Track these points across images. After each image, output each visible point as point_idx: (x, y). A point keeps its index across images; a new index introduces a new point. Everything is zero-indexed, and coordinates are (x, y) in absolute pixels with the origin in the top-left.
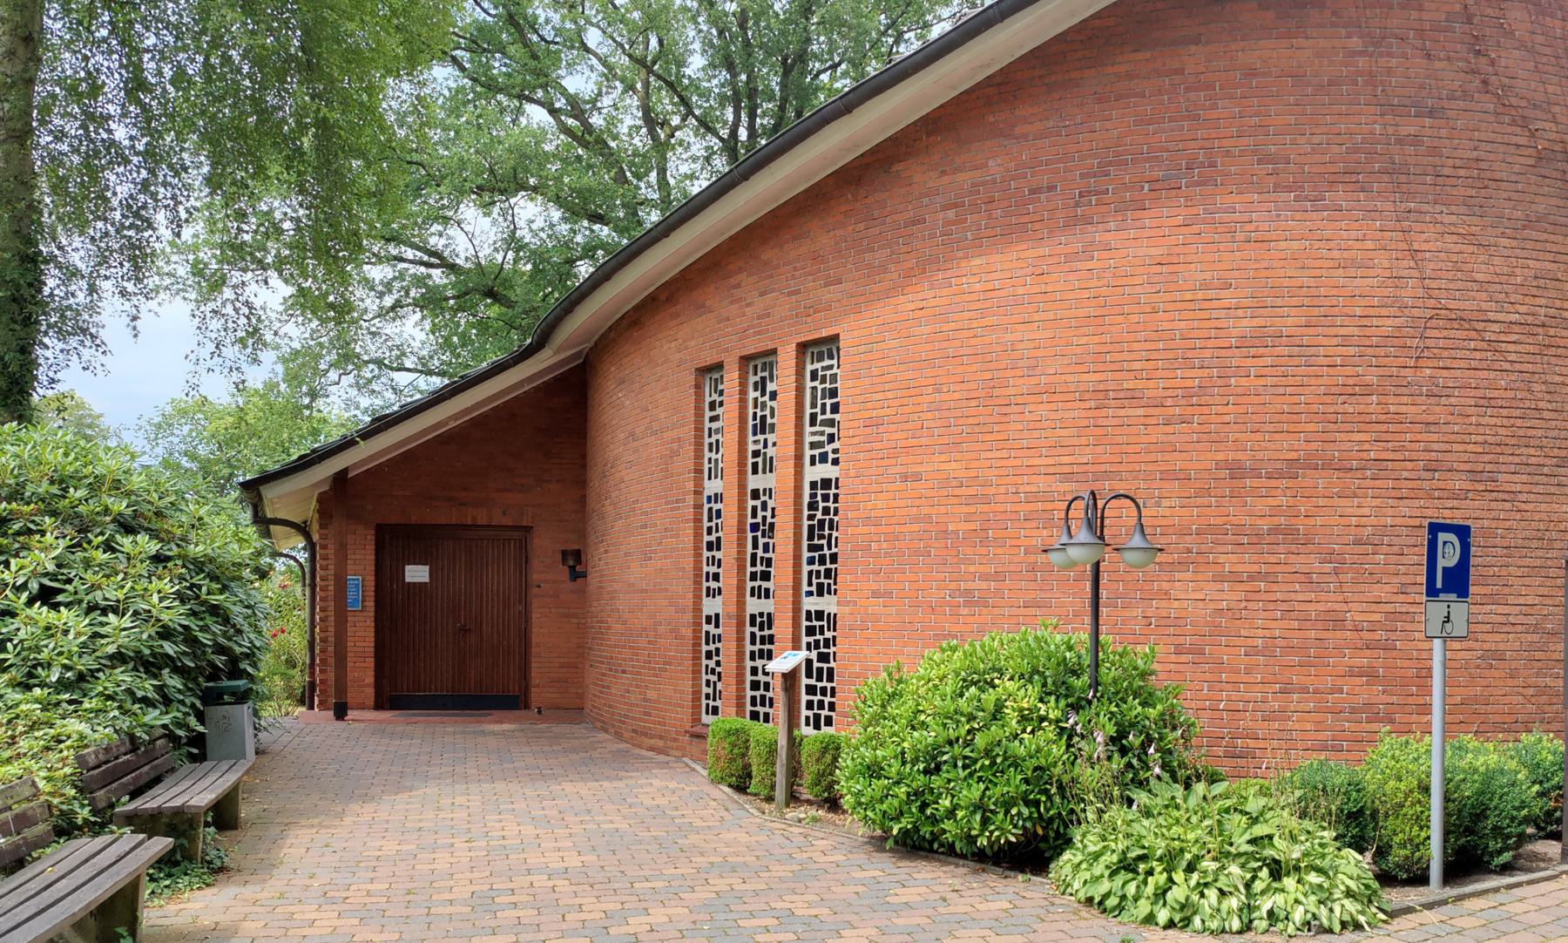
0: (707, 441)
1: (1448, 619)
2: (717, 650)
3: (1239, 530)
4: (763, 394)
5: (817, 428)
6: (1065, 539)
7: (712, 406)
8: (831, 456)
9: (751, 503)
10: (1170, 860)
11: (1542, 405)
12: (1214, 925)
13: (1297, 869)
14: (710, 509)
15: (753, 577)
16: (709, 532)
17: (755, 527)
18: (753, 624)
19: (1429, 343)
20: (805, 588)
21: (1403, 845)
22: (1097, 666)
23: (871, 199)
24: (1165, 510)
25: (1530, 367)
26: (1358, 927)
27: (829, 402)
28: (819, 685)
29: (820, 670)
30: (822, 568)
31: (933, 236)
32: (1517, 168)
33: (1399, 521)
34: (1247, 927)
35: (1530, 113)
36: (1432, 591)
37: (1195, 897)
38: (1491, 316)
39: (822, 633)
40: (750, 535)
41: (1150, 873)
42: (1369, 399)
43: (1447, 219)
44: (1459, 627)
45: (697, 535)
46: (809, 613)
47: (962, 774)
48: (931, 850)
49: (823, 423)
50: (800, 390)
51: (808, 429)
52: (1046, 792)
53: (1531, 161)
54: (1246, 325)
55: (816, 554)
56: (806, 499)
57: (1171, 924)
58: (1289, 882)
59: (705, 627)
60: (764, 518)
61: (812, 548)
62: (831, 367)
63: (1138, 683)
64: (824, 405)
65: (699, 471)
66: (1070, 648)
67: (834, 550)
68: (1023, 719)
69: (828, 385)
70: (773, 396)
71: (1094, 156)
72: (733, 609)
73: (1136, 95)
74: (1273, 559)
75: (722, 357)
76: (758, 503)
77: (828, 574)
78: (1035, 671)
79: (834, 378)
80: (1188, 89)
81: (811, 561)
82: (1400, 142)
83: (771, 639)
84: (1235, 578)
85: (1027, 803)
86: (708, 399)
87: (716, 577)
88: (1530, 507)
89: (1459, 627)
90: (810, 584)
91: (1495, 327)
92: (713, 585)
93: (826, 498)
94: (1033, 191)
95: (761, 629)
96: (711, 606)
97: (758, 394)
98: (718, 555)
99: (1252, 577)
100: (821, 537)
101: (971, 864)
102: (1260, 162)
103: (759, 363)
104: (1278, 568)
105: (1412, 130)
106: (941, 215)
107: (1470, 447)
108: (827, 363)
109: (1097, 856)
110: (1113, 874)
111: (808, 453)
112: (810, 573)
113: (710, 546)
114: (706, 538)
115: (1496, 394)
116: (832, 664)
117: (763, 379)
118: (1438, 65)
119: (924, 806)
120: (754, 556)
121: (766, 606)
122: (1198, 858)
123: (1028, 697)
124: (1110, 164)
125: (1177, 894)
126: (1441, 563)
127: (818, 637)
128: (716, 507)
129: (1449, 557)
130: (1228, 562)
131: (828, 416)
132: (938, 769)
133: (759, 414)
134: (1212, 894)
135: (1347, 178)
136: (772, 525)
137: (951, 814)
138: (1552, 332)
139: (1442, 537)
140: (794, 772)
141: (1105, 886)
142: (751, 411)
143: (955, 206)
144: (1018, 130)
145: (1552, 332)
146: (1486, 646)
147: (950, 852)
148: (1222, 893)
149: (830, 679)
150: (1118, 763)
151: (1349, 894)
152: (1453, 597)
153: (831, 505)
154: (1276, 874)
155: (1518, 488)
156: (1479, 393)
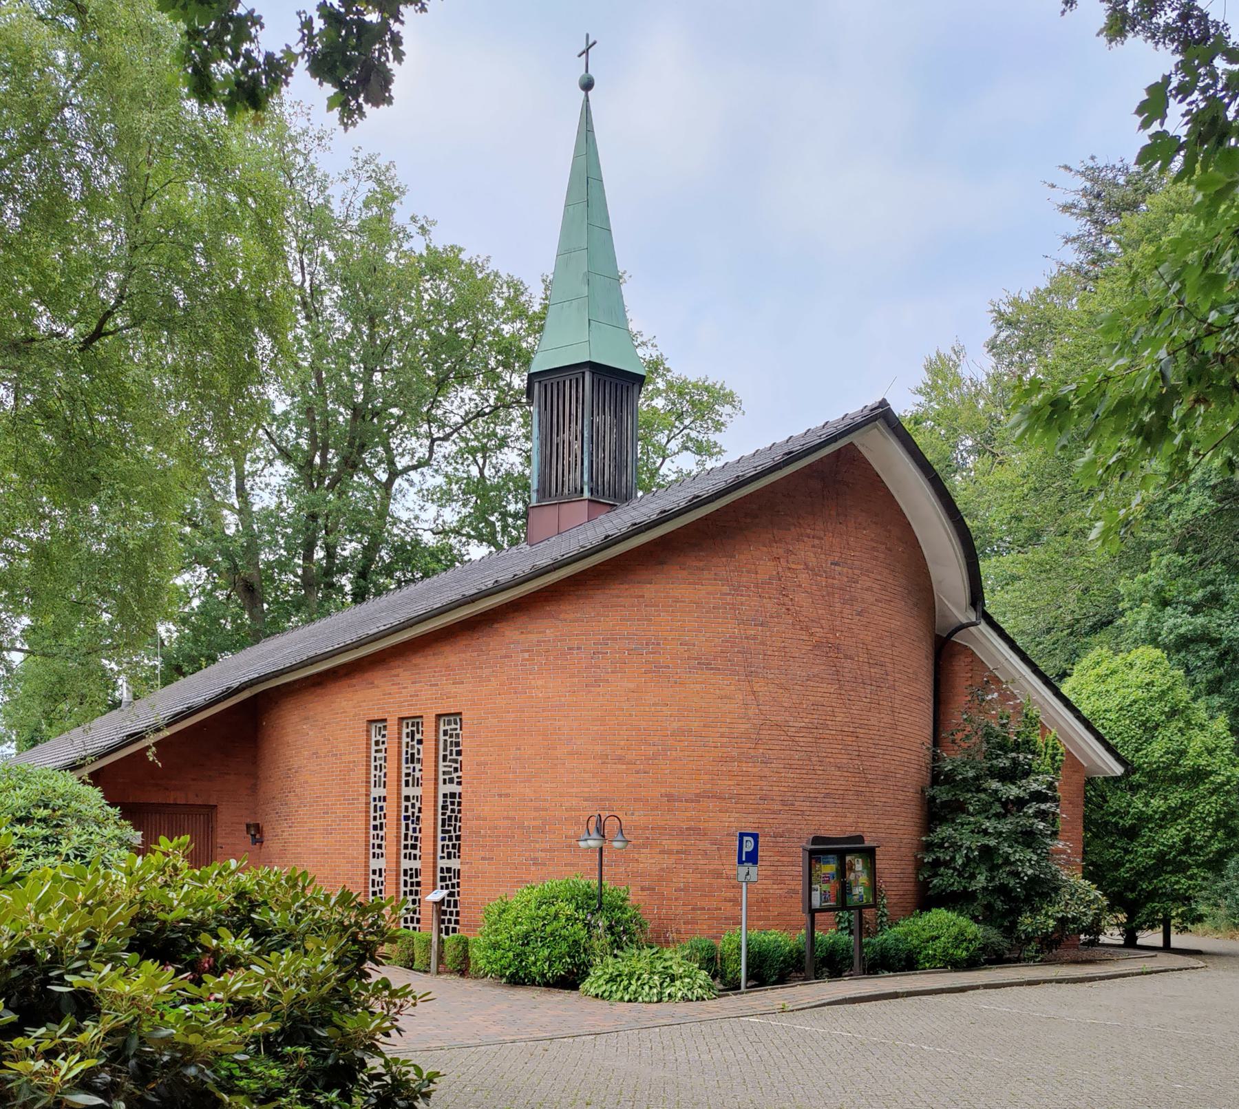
0: (373, 764)
1: (748, 874)
2: (458, 883)
4: (413, 740)
5: (447, 763)
6: (586, 836)
7: (377, 743)
9: (404, 804)
10: (630, 976)
11: (816, 767)
12: (647, 999)
13: (681, 977)
14: (375, 806)
15: (406, 847)
16: (375, 818)
17: (407, 818)
18: (405, 874)
19: (762, 737)
20: (440, 854)
21: (730, 973)
22: (601, 895)
23: (481, 640)
24: (635, 817)
25: (810, 749)
26: (704, 999)
27: (455, 749)
28: (449, 910)
29: (449, 901)
30: (450, 843)
31: (516, 665)
33: (748, 824)
34: (660, 1001)
35: (810, 624)
36: (741, 862)
37: (640, 989)
38: (791, 724)
39: (450, 880)
40: (403, 823)
41: (622, 980)
42: (733, 764)
44: (753, 877)
45: (367, 821)
46: (442, 869)
47: (540, 945)
48: (524, 984)
49: (451, 761)
50: (437, 740)
51: (441, 763)
53: (810, 648)
54: (675, 725)
55: (447, 835)
56: (440, 803)
57: (630, 1001)
58: (678, 983)
59: (372, 877)
60: (413, 813)
61: (443, 831)
62: (456, 729)
64: (451, 750)
66: (589, 887)
67: (458, 833)
68: (567, 919)
69: (454, 740)
71: (601, 634)
73: (621, 606)
76: (409, 804)
77: (454, 846)
80: (646, 606)
81: (443, 839)
82: (747, 638)
83: (418, 884)
84: (670, 852)
85: (570, 957)
86: (374, 739)
87: (380, 846)
88: (811, 818)
89: (753, 877)
90: (443, 852)
91: (793, 729)
92: (377, 851)
93: (452, 803)
94: (570, 649)
95: (411, 878)
96: (375, 864)
97: (409, 740)
98: (381, 833)
99: (678, 852)
101: (543, 988)
102: (681, 644)
103: (410, 722)
105: (753, 632)
106: (521, 655)
107: (782, 789)
108: (453, 726)
109: (600, 977)
110: (607, 983)
111: (441, 777)
112: (443, 846)
113: (375, 828)
114: (373, 823)
115: (794, 762)
116: (457, 898)
117: (413, 732)
119: (522, 961)
120: (406, 835)
121: (416, 864)
122: (641, 974)
123: (569, 909)
124: (608, 639)
125: (633, 988)
126: (745, 850)
127: (448, 882)
129: (749, 846)
130: (667, 843)
131: (454, 757)
132: (528, 944)
133: (410, 752)
134: (646, 988)
135: (722, 655)
136: (418, 818)
137: (534, 963)
138: (821, 731)
139: (745, 838)
140: (441, 958)
142: (404, 749)
143: (528, 651)
144: (561, 616)
145: (821, 731)
146: (790, 887)
147: (533, 983)
148: (651, 988)
149: (455, 906)
150: (609, 938)
151: (700, 987)
152: (750, 864)
153: (456, 808)
154: (673, 980)
155: (805, 808)
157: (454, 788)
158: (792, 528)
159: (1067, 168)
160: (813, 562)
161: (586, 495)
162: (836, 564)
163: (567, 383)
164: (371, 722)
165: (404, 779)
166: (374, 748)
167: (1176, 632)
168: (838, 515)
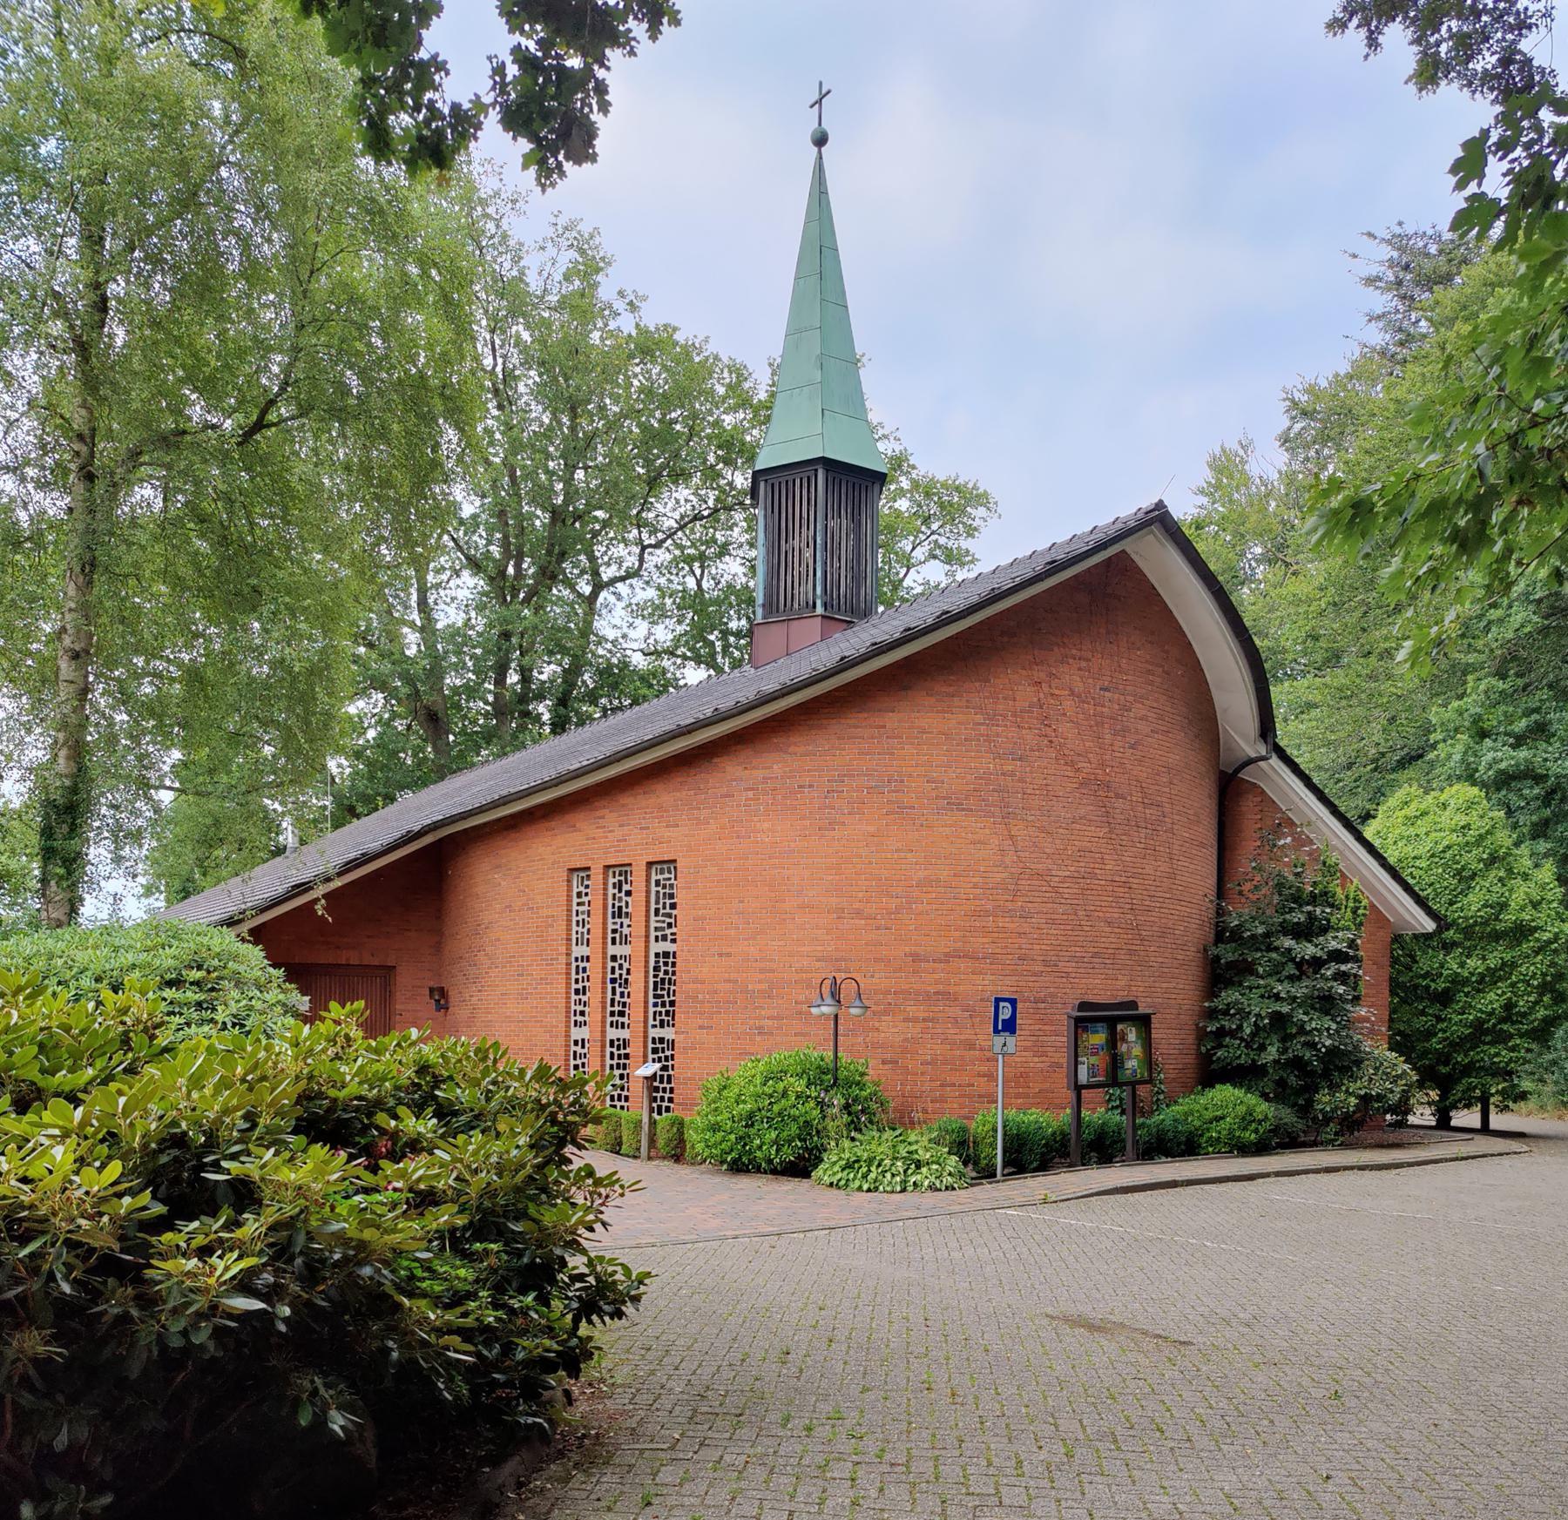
1: (1005, 1045)
3: (918, 993)
4: (620, 891)
5: (660, 918)
6: (819, 1002)
7: (579, 895)
8: (670, 937)
9: (610, 964)
10: (870, 1161)
14: (577, 967)
15: (612, 1014)
17: (613, 981)
20: (651, 1022)
24: (876, 980)
25: (1076, 902)
26: (954, 1189)
30: (663, 1010)
32: (1068, 790)
34: (904, 1190)
35: (1076, 758)
36: (996, 1031)
37: (880, 1177)
38: (1054, 873)
39: (663, 1052)
40: (609, 986)
41: (860, 1167)
43: (1031, 818)
45: (568, 984)
46: (654, 1039)
47: (766, 1126)
49: (663, 915)
50: (648, 892)
51: (653, 918)
52: (810, 1134)
57: (869, 1190)
58: (924, 1170)
59: (573, 1048)
60: (621, 975)
61: (656, 996)
63: (858, 1078)
65: (569, 940)
68: (798, 1097)
69: (667, 891)
70: (628, 893)
72: (598, 1035)
74: (936, 1009)
75: (589, 864)
76: (616, 965)
77: (667, 1013)
78: (804, 1072)
79: (671, 886)
81: (655, 1005)
82: (1003, 774)
83: (627, 1056)
84: (915, 1020)
85: (800, 1140)
86: (575, 890)
87: (582, 1013)
89: (1011, 1048)
90: (655, 1020)
91: (1057, 879)
92: (579, 1018)
93: (666, 964)
94: (800, 787)
95: (618, 1049)
96: (577, 1034)
97: (616, 891)
100: (662, 989)
104: (940, 1015)
105: (1010, 768)
106: (744, 794)
108: (667, 875)
110: (843, 1170)
111: (653, 934)
112: (655, 1013)
113: (577, 992)
114: (574, 986)
116: (671, 1072)
118: (1024, 732)
119: (745, 1145)
120: (613, 1001)
121: (624, 1034)
122: (882, 1160)
123: (800, 1085)
125: (872, 1176)
126: (1001, 1017)
128: (582, 965)
129: (1005, 1014)
130: (912, 1010)
132: (752, 1125)
134: (888, 1175)
136: (626, 980)
137: (760, 1148)
141: (839, 1176)
142: (610, 902)
143: (753, 789)
147: (758, 1170)
148: (893, 1175)
149: (669, 1082)
151: (950, 1174)
153: (670, 968)
154: (918, 1167)
156: (1049, 916)
157: (667, 946)
158: (1056, 649)
159: (1370, 235)
160: (1079, 687)
161: (819, 610)
162: (1106, 690)
163: (790, 484)
164: (572, 870)
165: (610, 935)
166: (575, 900)
167: (1496, 767)
168: (1108, 633)
